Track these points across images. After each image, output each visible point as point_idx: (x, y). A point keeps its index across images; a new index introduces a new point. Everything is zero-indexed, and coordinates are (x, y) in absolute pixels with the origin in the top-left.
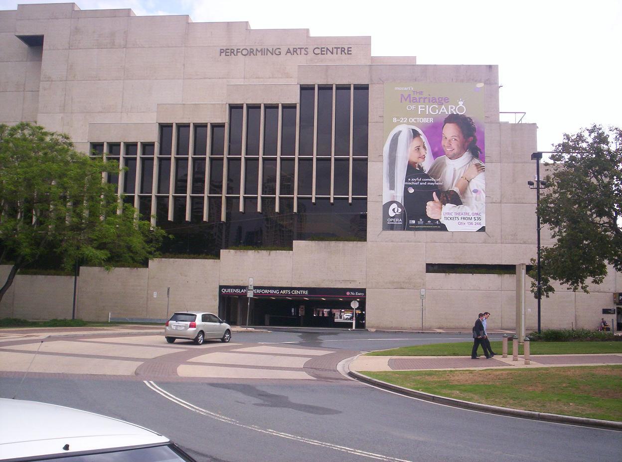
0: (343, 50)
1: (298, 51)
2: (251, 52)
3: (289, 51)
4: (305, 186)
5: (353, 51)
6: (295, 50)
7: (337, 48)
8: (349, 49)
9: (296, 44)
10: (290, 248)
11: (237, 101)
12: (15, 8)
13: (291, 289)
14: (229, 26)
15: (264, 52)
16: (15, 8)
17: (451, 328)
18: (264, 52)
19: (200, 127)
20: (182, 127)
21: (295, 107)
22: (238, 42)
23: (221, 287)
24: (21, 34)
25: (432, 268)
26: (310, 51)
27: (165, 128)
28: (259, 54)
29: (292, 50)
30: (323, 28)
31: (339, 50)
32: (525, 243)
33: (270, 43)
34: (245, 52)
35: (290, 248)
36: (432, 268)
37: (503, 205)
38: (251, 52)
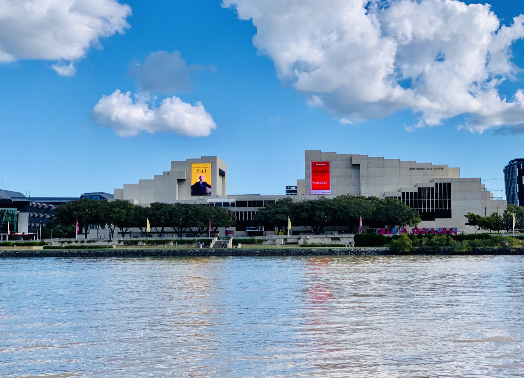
2: (417, 169)
4: (437, 206)
15: (420, 169)
18: (420, 169)
38: (417, 169)
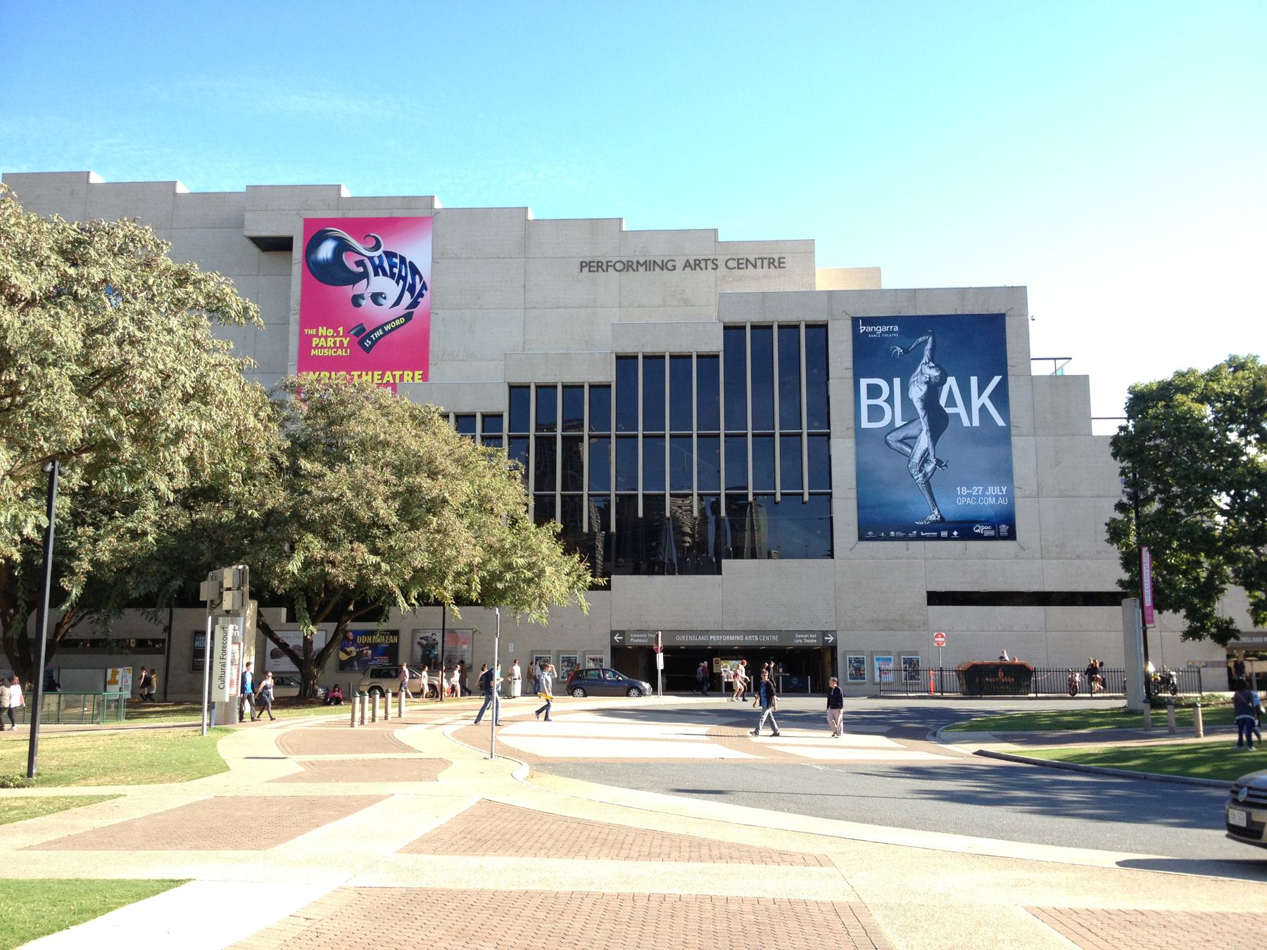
0: (771, 262)
1: (703, 264)
2: (628, 266)
3: (687, 264)
5: (788, 262)
6: (697, 264)
7: (762, 259)
8: (710, 265)
9: (702, 255)
10: (719, 571)
11: (628, 349)
12: (244, 190)
13: (707, 632)
14: (594, 225)
15: (649, 265)
16: (244, 190)
17: (1257, 789)
18: (649, 265)
19: (573, 390)
20: (546, 390)
21: (717, 356)
22: (606, 251)
23: (613, 633)
24: (255, 234)
25: (936, 598)
26: (721, 263)
27: (517, 392)
28: (642, 269)
29: (692, 263)
30: (740, 226)
31: (766, 263)
32: (1078, 557)
33: (658, 252)
34: (619, 266)
35: (719, 571)
36: (936, 598)
37: (1041, 500)
38: (628, 266)
